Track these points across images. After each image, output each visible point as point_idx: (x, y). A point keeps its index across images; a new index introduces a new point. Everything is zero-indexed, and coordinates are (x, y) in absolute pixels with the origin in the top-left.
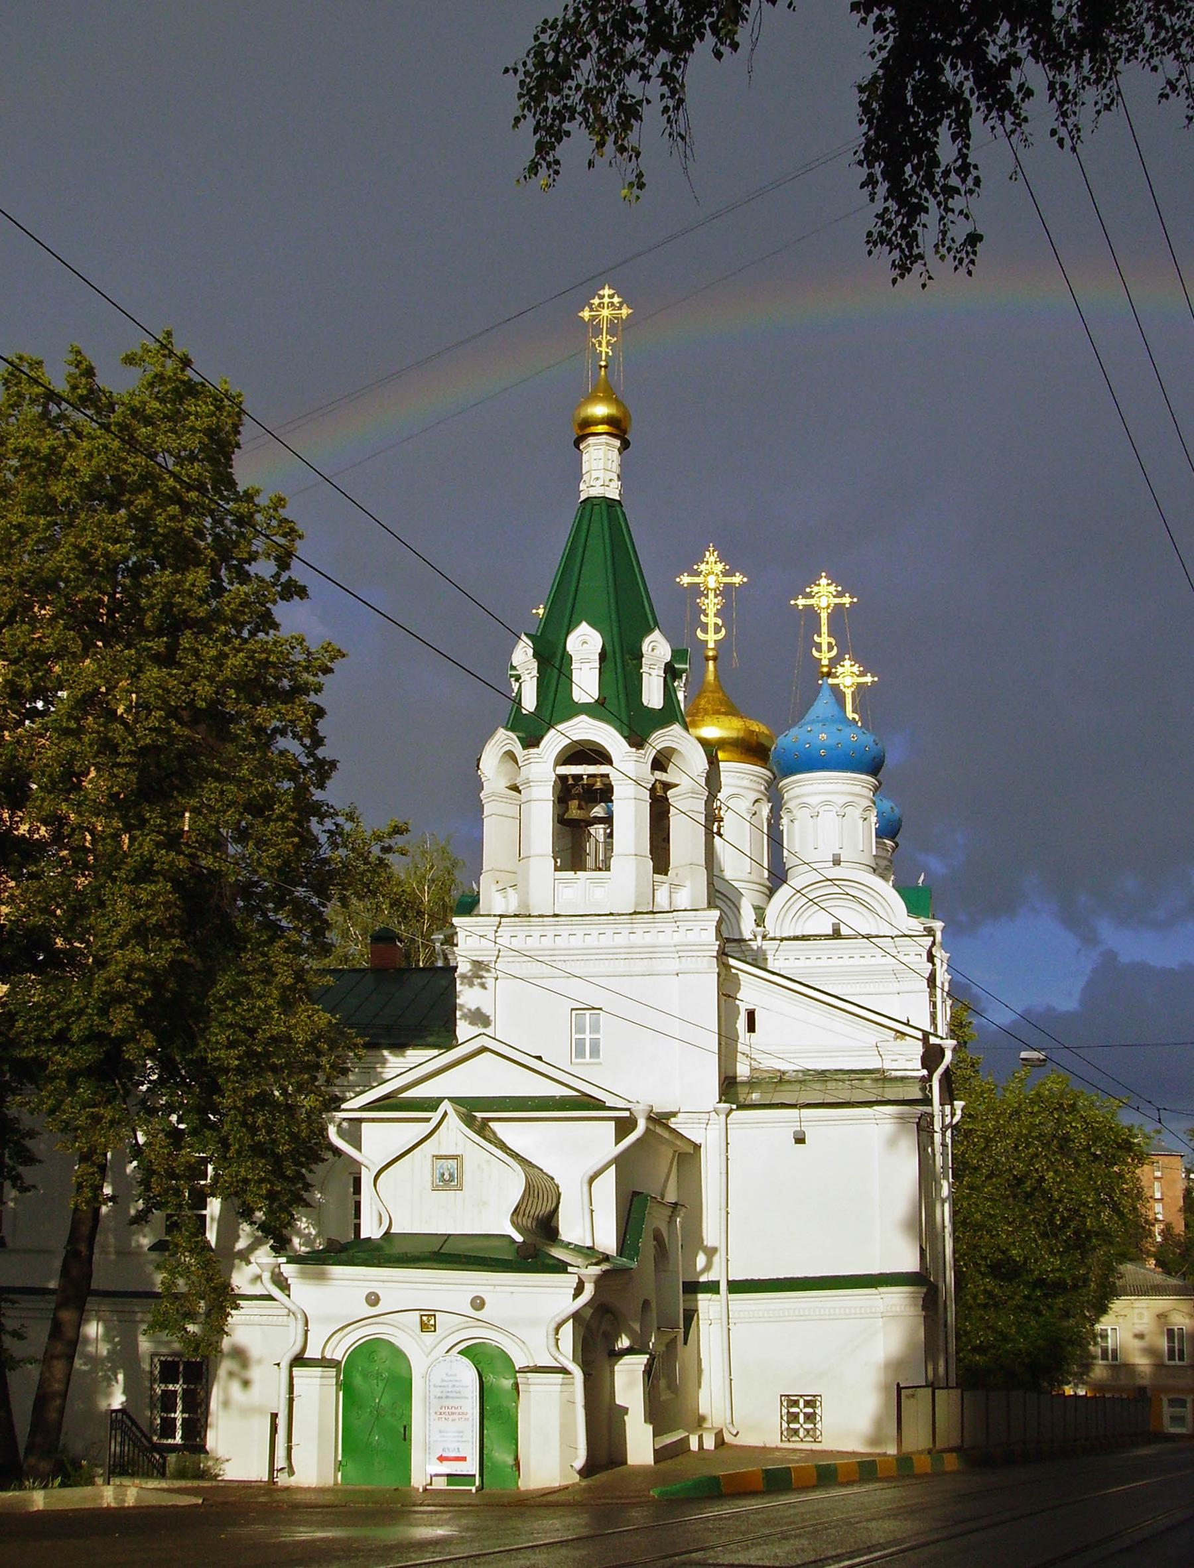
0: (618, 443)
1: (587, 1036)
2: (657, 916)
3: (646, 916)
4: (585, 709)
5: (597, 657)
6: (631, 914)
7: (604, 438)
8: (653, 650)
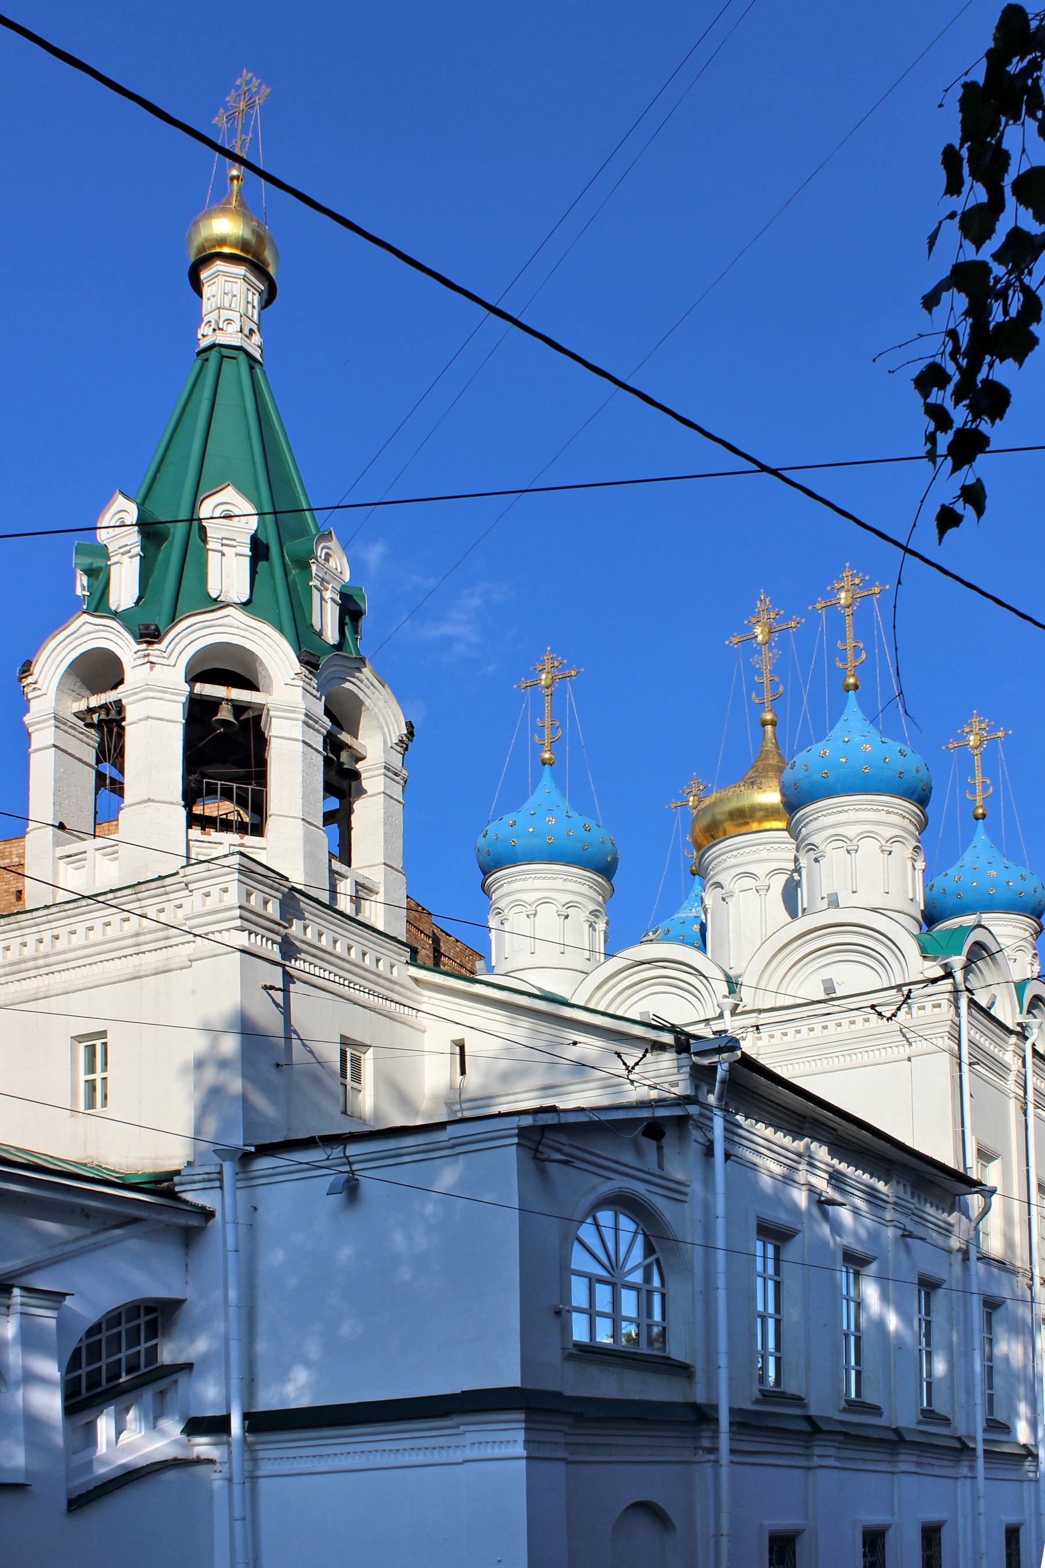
0: (241, 270)
1: (98, 1076)
2: (168, 881)
3: (154, 885)
6: (134, 885)
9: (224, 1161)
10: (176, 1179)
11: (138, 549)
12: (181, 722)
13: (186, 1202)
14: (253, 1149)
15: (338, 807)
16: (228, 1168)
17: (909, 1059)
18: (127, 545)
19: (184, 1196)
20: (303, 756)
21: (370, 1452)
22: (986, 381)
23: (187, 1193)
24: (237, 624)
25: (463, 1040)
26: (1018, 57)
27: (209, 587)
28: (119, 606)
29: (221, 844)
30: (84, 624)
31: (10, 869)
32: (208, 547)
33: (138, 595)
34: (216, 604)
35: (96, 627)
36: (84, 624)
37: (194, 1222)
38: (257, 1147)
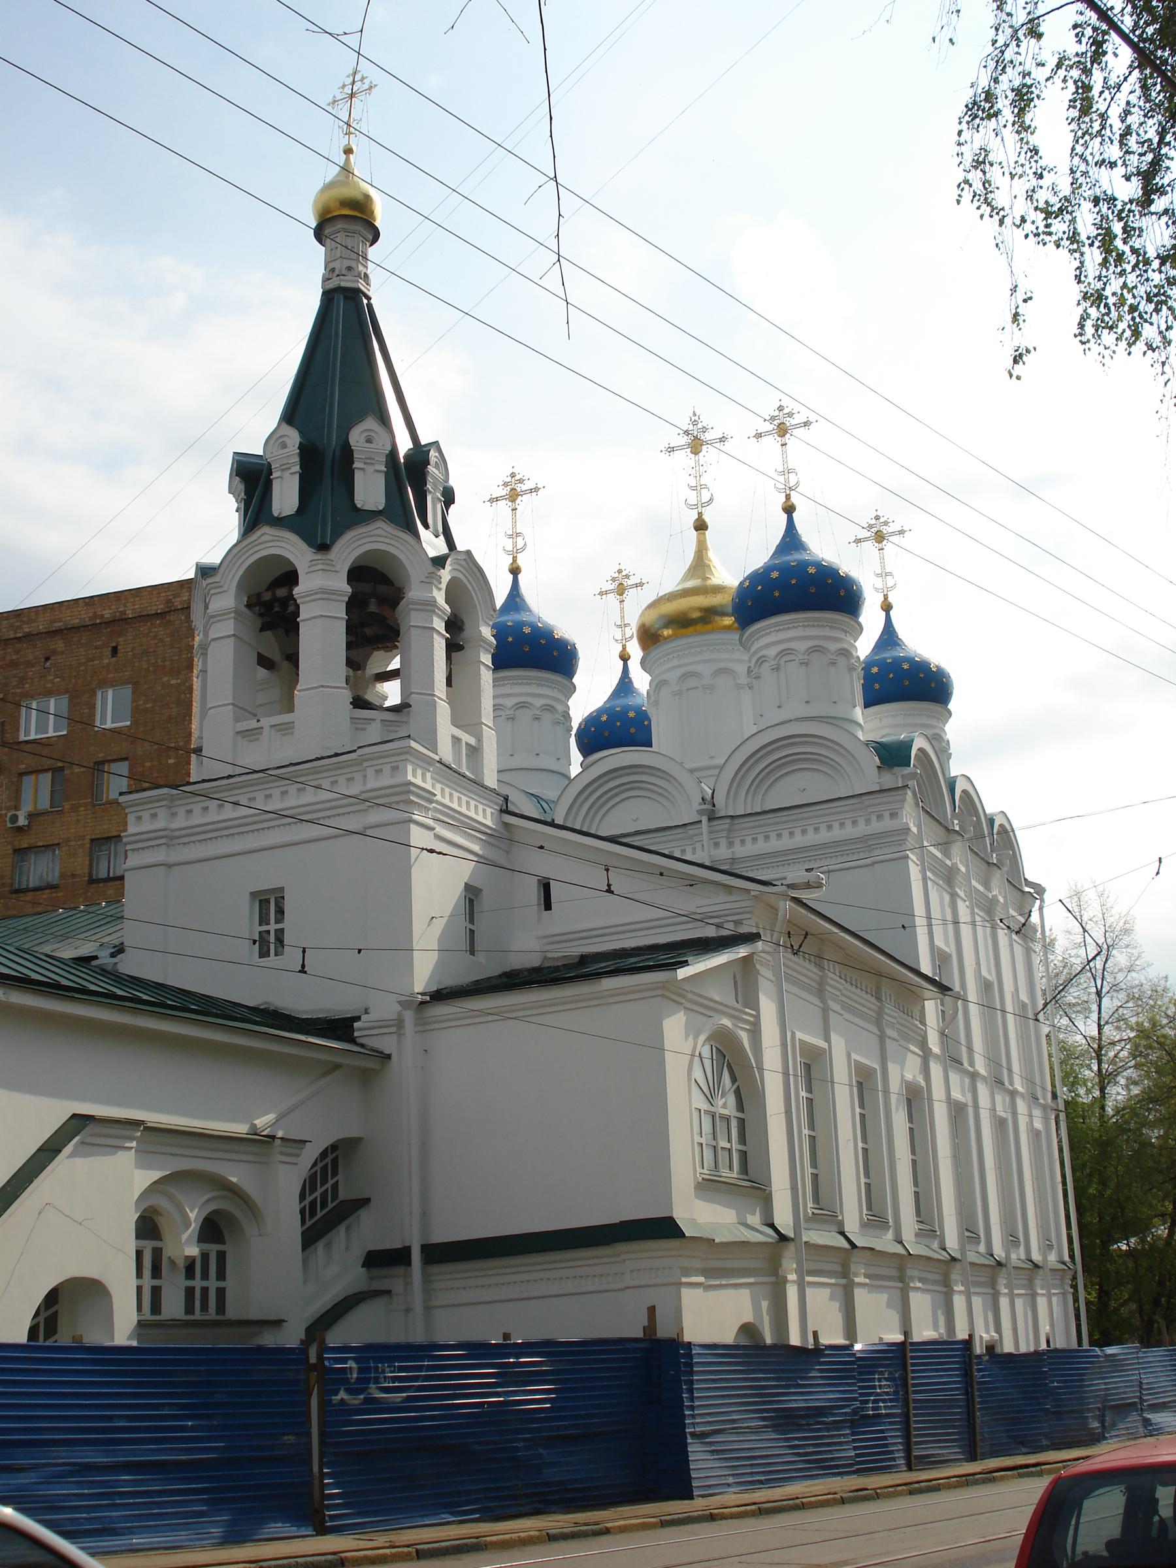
4: (280, 522)
5: (297, 459)
7: (340, 225)
8: (369, 441)
9: (405, 1010)
10: (356, 1025)
11: (297, 468)
12: (342, 618)
13: (362, 1046)
14: (428, 998)
15: (193, 576)
16: (409, 1017)
17: (360, 951)
18: (288, 463)
19: (359, 1040)
20: (354, 604)
21: (535, 1281)
22: (1087, 1418)
23: (367, 1038)
24: (384, 534)
25: (282, 889)
26: (1077, 1510)
27: (355, 498)
28: (280, 513)
29: (374, 720)
30: (263, 535)
31: (624, 840)
32: (354, 466)
33: (297, 505)
34: (367, 516)
35: (274, 538)
36: (263, 535)
37: (371, 1064)
38: (430, 996)
